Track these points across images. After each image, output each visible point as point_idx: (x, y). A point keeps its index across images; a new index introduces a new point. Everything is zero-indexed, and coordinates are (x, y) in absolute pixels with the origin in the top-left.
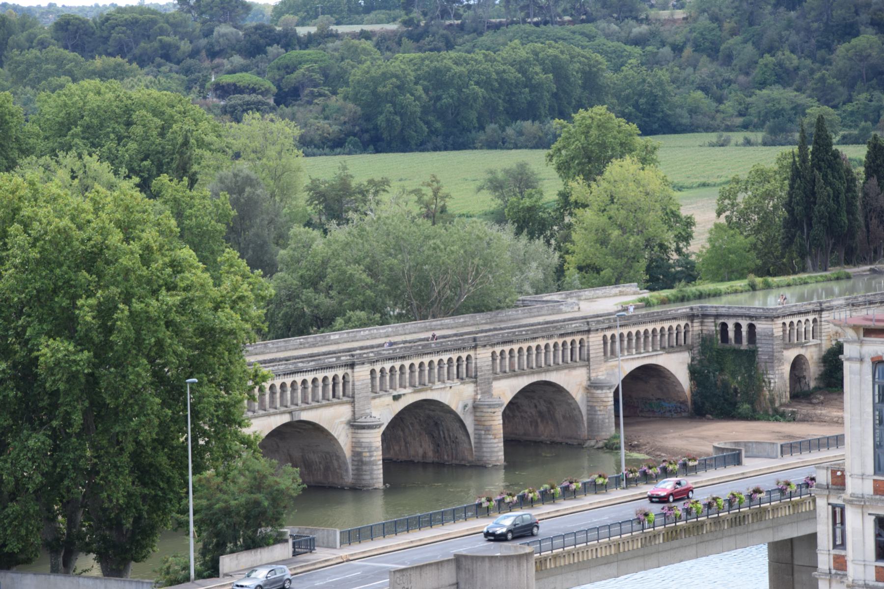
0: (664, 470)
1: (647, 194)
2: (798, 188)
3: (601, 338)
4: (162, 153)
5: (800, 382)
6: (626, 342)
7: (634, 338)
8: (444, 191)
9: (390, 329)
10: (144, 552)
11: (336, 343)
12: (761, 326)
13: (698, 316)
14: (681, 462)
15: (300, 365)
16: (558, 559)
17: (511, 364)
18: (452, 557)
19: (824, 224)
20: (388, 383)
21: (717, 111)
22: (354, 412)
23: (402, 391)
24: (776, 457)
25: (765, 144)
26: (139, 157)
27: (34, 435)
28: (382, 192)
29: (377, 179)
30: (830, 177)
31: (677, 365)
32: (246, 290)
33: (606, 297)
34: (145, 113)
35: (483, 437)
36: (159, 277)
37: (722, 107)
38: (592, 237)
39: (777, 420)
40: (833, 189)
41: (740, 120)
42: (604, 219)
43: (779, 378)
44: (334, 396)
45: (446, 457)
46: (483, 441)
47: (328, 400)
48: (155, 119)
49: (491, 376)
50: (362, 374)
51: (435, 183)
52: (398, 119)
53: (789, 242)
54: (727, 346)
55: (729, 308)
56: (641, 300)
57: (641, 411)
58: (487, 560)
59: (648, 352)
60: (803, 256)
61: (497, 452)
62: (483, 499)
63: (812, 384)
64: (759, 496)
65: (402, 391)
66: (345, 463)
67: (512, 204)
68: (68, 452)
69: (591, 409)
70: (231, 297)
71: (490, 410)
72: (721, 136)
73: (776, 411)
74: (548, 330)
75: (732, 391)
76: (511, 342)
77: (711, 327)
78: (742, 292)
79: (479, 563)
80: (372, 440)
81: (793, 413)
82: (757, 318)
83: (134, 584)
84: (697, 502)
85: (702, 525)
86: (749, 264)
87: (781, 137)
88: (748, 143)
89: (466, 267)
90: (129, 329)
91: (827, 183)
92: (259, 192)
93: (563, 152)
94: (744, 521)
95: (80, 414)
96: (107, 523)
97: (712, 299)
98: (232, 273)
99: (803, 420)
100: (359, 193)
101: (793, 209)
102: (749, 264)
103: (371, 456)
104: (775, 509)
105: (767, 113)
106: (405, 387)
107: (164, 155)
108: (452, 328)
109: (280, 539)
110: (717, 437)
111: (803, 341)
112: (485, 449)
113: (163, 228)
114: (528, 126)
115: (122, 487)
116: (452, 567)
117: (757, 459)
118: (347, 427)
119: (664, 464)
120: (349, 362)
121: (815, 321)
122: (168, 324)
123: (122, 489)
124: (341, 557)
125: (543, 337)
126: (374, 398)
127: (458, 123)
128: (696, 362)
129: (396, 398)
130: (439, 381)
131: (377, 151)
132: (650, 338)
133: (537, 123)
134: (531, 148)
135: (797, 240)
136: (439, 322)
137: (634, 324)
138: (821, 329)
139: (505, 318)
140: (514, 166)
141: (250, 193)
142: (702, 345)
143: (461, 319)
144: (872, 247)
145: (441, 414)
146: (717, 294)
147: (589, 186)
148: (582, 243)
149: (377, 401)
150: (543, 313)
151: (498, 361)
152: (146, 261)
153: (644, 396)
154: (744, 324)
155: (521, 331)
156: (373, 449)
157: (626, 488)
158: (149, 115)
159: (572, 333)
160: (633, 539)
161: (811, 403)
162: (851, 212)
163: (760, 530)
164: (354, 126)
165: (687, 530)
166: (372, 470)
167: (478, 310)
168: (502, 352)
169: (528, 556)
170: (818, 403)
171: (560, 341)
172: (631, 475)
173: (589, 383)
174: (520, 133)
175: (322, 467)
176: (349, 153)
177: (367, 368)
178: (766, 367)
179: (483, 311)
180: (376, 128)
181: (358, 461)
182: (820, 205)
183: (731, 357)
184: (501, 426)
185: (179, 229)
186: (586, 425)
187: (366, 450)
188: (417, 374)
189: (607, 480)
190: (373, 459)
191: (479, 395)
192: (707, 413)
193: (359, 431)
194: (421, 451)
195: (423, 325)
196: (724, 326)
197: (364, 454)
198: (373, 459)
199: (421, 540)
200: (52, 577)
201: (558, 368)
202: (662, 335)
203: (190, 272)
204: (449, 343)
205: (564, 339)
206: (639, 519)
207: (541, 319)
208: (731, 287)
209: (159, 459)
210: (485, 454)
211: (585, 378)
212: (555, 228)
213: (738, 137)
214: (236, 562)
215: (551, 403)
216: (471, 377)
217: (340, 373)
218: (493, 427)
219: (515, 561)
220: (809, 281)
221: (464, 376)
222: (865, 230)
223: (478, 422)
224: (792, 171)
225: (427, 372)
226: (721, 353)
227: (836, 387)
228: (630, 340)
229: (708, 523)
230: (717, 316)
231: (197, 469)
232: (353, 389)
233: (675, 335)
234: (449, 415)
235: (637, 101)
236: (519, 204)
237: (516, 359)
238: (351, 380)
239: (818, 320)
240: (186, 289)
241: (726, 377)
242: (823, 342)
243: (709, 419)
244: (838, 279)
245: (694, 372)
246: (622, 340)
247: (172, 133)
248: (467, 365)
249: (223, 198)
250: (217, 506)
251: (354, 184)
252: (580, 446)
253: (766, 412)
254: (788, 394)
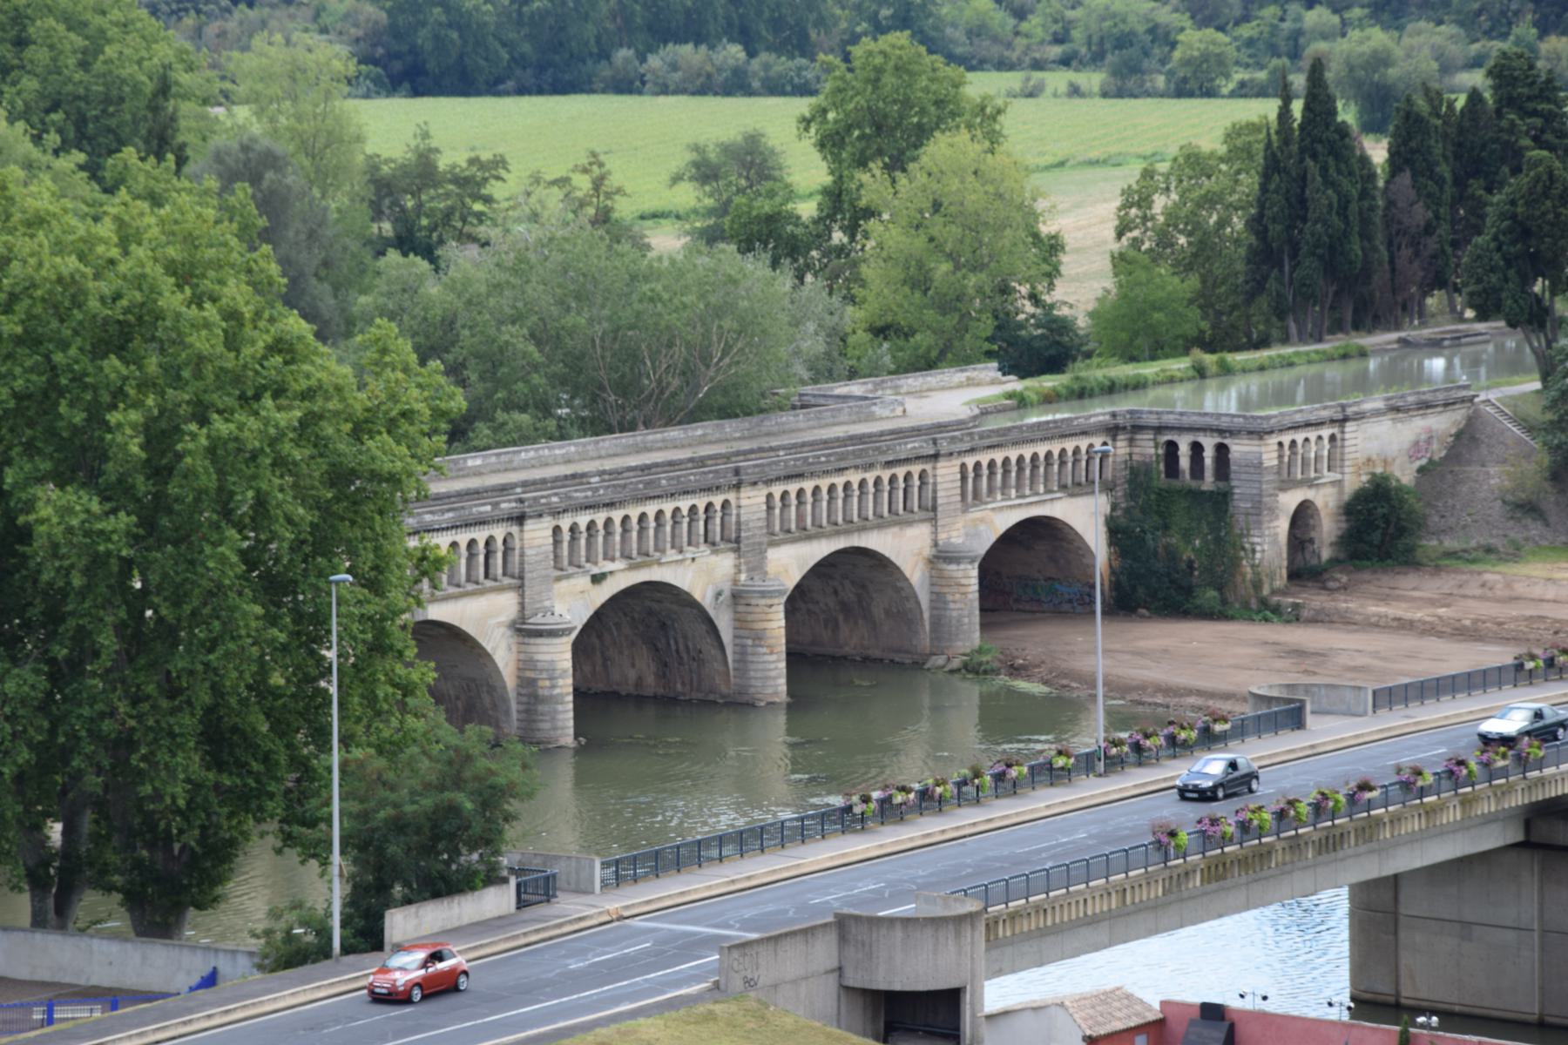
0: (1172, 740)
1: (1000, 196)
2: (1276, 192)
3: (957, 469)
4: (86, 99)
5: (1303, 549)
6: (999, 477)
7: (1014, 469)
8: (615, 181)
9: (573, 449)
10: (219, 890)
11: (477, 472)
12: (1239, 449)
13: (1124, 428)
14: (1200, 724)
15: (428, 518)
16: (1017, 921)
17: (800, 517)
18: (830, 919)
19: (1321, 257)
20: (583, 552)
21: (1017, 34)
22: (522, 605)
23: (608, 566)
24: (1364, 714)
25: (1105, 95)
26: (42, 105)
27: (16, 671)
28: (493, 182)
29: (486, 156)
30: (1332, 171)
31: (1086, 517)
32: (416, 400)
33: (943, 389)
34: (54, 23)
35: (749, 650)
36: (257, 373)
37: (1025, 26)
38: (897, 273)
39: (1266, 620)
40: (1339, 193)
41: (1056, 51)
42: (920, 242)
43: (1269, 543)
44: (487, 576)
45: (679, 687)
46: (750, 658)
47: (477, 583)
48: (72, 36)
49: (765, 540)
50: (537, 534)
51: (595, 168)
52: (455, 35)
53: (1257, 286)
54: (1176, 483)
55: (1182, 414)
56: (1010, 396)
57: (1017, 601)
58: (898, 926)
59: (1037, 494)
60: (1281, 314)
61: (775, 678)
62: (855, 799)
63: (1326, 554)
64: (1368, 795)
65: (608, 566)
66: (505, 700)
67: (738, 206)
68: (80, 705)
69: (938, 599)
70: (386, 413)
71: (763, 602)
72: (1028, 79)
73: (1264, 603)
74: (862, 450)
75: (1183, 566)
76: (800, 476)
77: (1148, 448)
78: (1181, 380)
79: (883, 931)
80: (555, 657)
81: (1296, 606)
82: (1232, 432)
83: (199, 953)
84: (1260, 808)
85: (1269, 853)
86: (1187, 327)
87: (1131, 84)
88: (1075, 91)
89: (706, 335)
90: (207, 472)
91: (1329, 183)
92: (289, 180)
93: (831, 116)
94: (1342, 843)
95: (112, 633)
96: (148, 836)
97: (1130, 393)
98: (386, 364)
99: (1314, 621)
100: (451, 181)
101: (1266, 230)
102: (1187, 327)
103: (553, 687)
104: (1396, 820)
105: (1102, 38)
106: (613, 559)
107: (87, 103)
108: (683, 446)
109: (493, 878)
110: (1166, 651)
111: (1313, 475)
112: (752, 674)
113: (256, 278)
114: (686, 52)
115: (180, 772)
116: (832, 937)
117: (1328, 718)
118: (509, 633)
119: (1171, 729)
120: (516, 513)
121: (1332, 438)
122: (280, 463)
123: (182, 776)
124: (608, 912)
125: (856, 467)
126: (558, 579)
127: (561, 44)
128: (1119, 513)
129: (597, 579)
130: (673, 547)
131: (417, 92)
132: (1042, 470)
133: (703, 48)
134: (693, 94)
135: (1272, 285)
136: (659, 436)
137: (1015, 443)
138: (1342, 454)
139: (775, 429)
140: (739, 138)
141: (272, 181)
142: (1130, 482)
143: (698, 430)
144: (1399, 299)
145: (675, 607)
146: (1138, 385)
147: (894, 181)
148: (880, 286)
149: (564, 584)
150: (842, 419)
151: (777, 511)
152: (232, 342)
153: (1026, 572)
154: (1209, 443)
155: (818, 457)
156: (558, 673)
157: (1106, 773)
158: (61, 28)
159: (907, 461)
160: (1149, 879)
161: (1325, 588)
162: (1366, 236)
163: (1358, 855)
164: (374, 45)
165: (1243, 863)
166: (556, 712)
167: (726, 413)
168: (785, 495)
169: (971, 917)
170: (1338, 589)
171: (886, 475)
172: (1114, 751)
173: (934, 551)
174: (674, 67)
175: (460, 704)
176: (367, 96)
177: (547, 523)
178: (1247, 523)
179: (737, 416)
180: (414, 50)
181: (529, 695)
182: (1316, 222)
183: (1185, 504)
184: (783, 631)
185: (285, 281)
186: (927, 627)
187: (544, 675)
188: (634, 535)
189: (1072, 760)
190: (557, 691)
191: (740, 572)
192: (1139, 606)
193: (532, 641)
194: (632, 675)
195: (631, 441)
196: (1172, 447)
197: (541, 683)
198: (557, 691)
199: (749, 878)
200: (39, 937)
201: (881, 524)
202: (1062, 463)
203: (313, 363)
204: (692, 477)
205: (893, 471)
206: (1159, 841)
207: (839, 432)
208: (1163, 371)
209: (252, 718)
210: (753, 682)
211: (928, 542)
212: (814, 253)
213: (1058, 80)
214: (414, 922)
215: (863, 587)
216: (729, 541)
217: (499, 532)
218: (768, 633)
219: (951, 927)
220: (1295, 360)
221: (718, 538)
222: (1387, 266)
223: (741, 623)
224: (1265, 158)
225: (651, 532)
226: (1165, 496)
227: (1369, 559)
228: (1006, 472)
229: (1279, 846)
230: (1159, 429)
231: (346, 741)
232: (522, 563)
233: (1084, 463)
234: (688, 610)
235: (876, 13)
236: (751, 208)
237: (809, 507)
238: (518, 546)
239: (1339, 436)
240: (307, 395)
241: (1174, 541)
242: (1347, 477)
243: (1142, 617)
244: (1345, 357)
245: (1116, 532)
246: (992, 473)
247: (105, 62)
248: (722, 519)
249: (241, 195)
250: (382, 814)
251: (443, 163)
252: (918, 665)
253: (1246, 605)
254: (1284, 572)
